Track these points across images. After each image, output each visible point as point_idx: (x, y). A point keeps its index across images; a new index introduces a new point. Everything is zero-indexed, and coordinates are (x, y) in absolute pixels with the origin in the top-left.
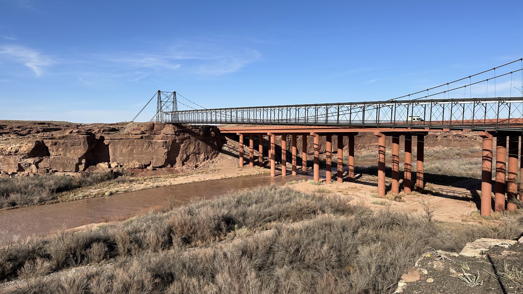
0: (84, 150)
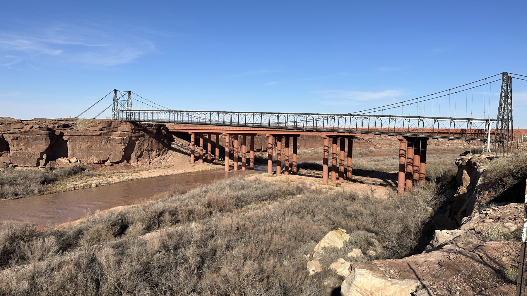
0: (46, 145)
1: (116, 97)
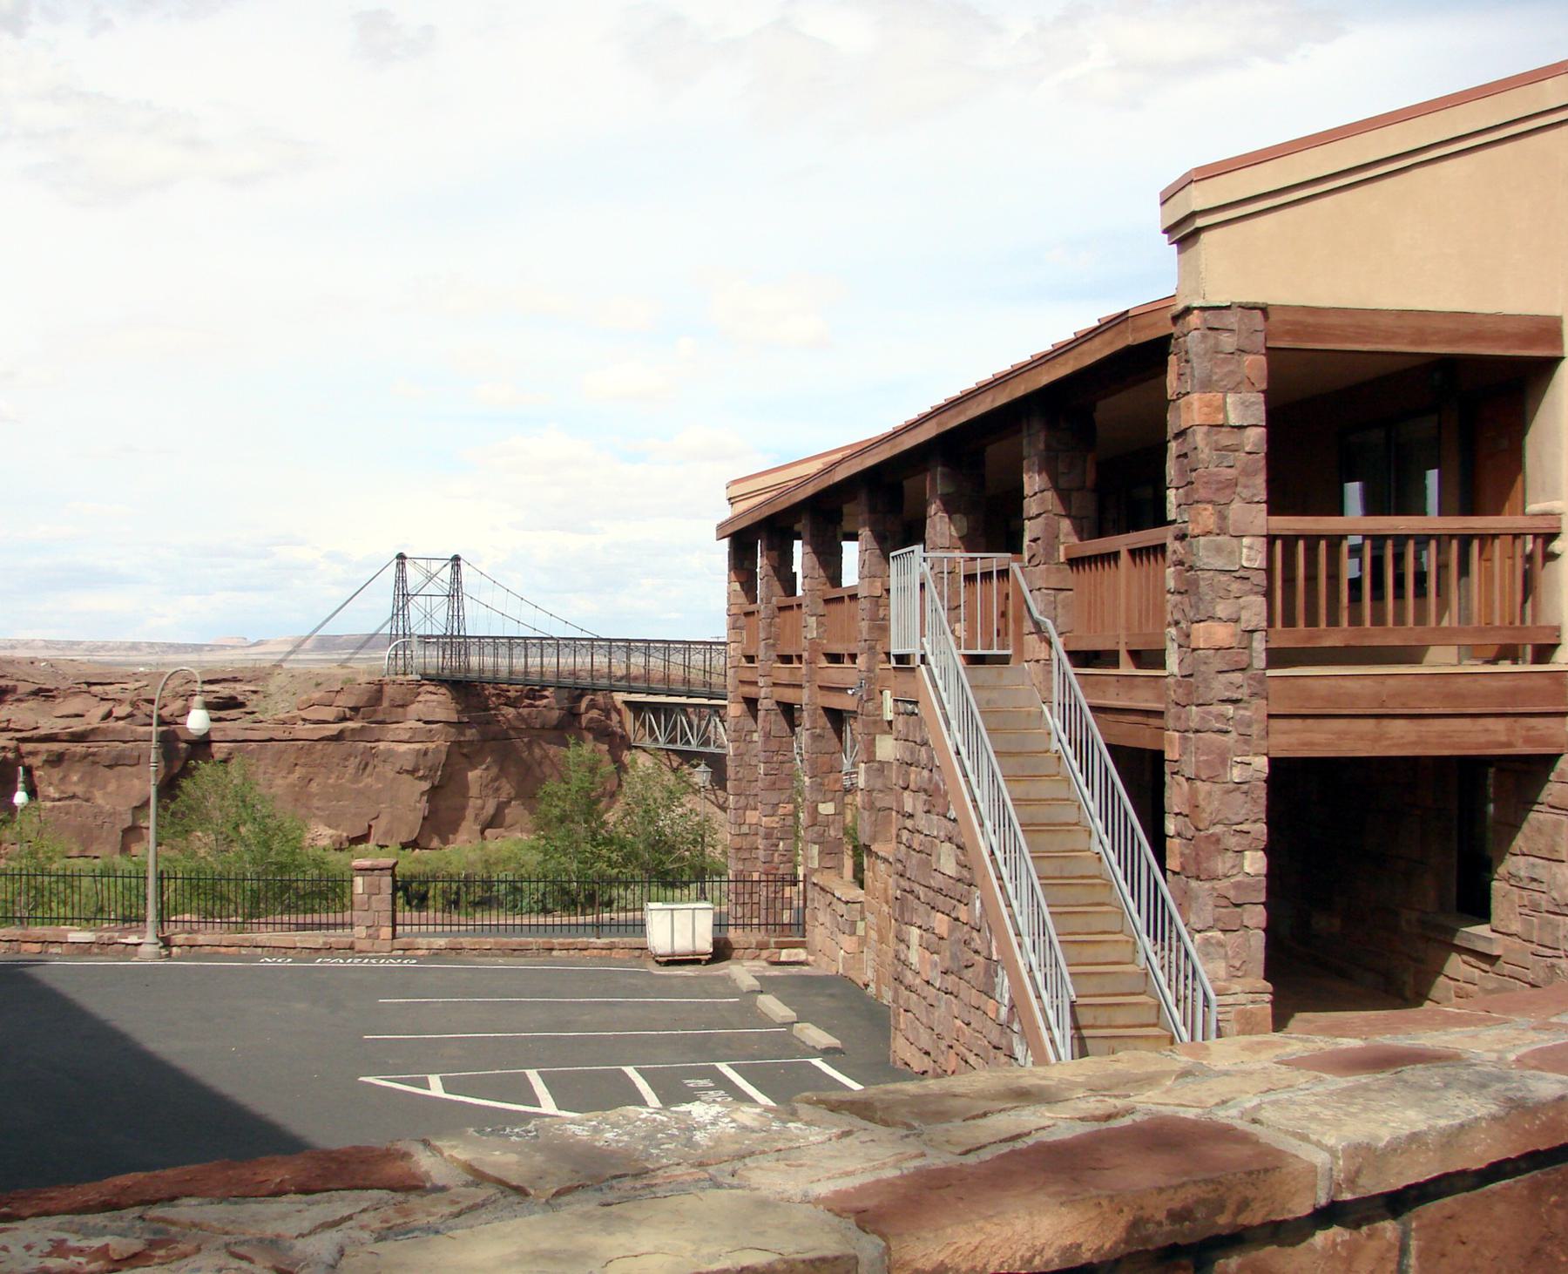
1: (405, 581)
